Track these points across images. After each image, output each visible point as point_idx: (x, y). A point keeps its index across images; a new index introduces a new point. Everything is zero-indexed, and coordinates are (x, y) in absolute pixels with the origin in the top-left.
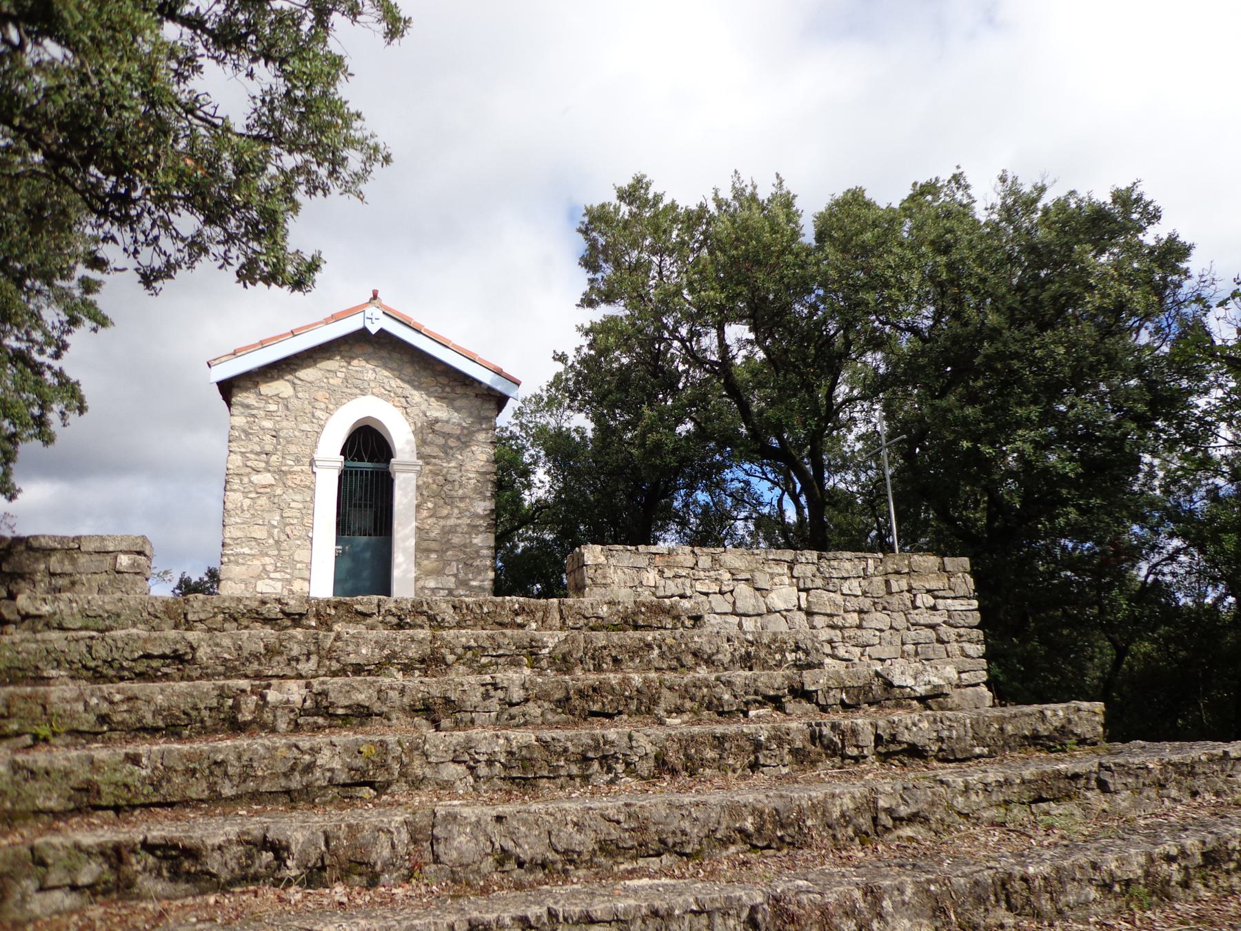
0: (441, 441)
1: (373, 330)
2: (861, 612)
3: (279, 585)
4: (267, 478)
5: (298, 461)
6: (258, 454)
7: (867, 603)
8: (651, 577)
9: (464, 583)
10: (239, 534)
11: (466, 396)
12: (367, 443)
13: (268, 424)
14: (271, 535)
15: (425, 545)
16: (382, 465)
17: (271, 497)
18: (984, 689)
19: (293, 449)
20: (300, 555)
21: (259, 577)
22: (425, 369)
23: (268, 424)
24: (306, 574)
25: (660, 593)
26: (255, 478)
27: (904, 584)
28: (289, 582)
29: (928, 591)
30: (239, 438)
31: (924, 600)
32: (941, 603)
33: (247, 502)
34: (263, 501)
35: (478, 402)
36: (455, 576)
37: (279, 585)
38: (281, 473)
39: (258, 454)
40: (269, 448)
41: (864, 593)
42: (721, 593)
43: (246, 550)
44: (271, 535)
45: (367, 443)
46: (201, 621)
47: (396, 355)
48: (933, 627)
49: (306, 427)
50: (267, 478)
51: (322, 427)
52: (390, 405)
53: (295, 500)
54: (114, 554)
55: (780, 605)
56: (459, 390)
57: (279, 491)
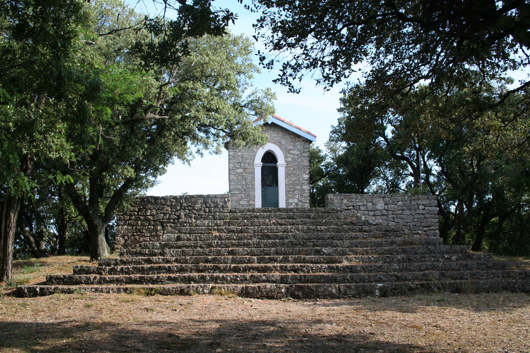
0: (292, 156)
1: (270, 123)
2: (403, 210)
3: (246, 202)
4: (240, 170)
5: (249, 165)
6: (238, 163)
7: (404, 208)
8: (345, 201)
9: (300, 201)
10: (234, 187)
11: (299, 141)
12: (269, 158)
13: (240, 154)
14: (243, 188)
15: (288, 190)
16: (273, 165)
17: (242, 176)
18: (438, 231)
19: (247, 161)
20: (251, 193)
21: (240, 200)
22: (286, 133)
23: (240, 154)
24: (253, 199)
25: (348, 205)
26: (237, 170)
27: (415, 203)
28: (249, 201)
29: (423, 205)
30: (232, 159)
31: (421, 207)
32: (426, 208)
33: (236, 178)
34: (240, 177)
35: (303, 143)
36: (298, 199)
37: (246, 202)
38: (245, 169)
39: (238, 163)
40: (241, 161)
41: (404, 205)
42: (364, 205)
43: (236, 192)
44: (243, 188)
45: (269, 158)
46: (423, 205)
47: (277, 129)
48: (424, 214)
49: (251, 154)
50: (240, 170)
51: (256, 154)
52: (275, 146)
53: (249, 177)
54: (224, 198)
55: (380, 208)
56: (297, 139)
57: (244, 174)
